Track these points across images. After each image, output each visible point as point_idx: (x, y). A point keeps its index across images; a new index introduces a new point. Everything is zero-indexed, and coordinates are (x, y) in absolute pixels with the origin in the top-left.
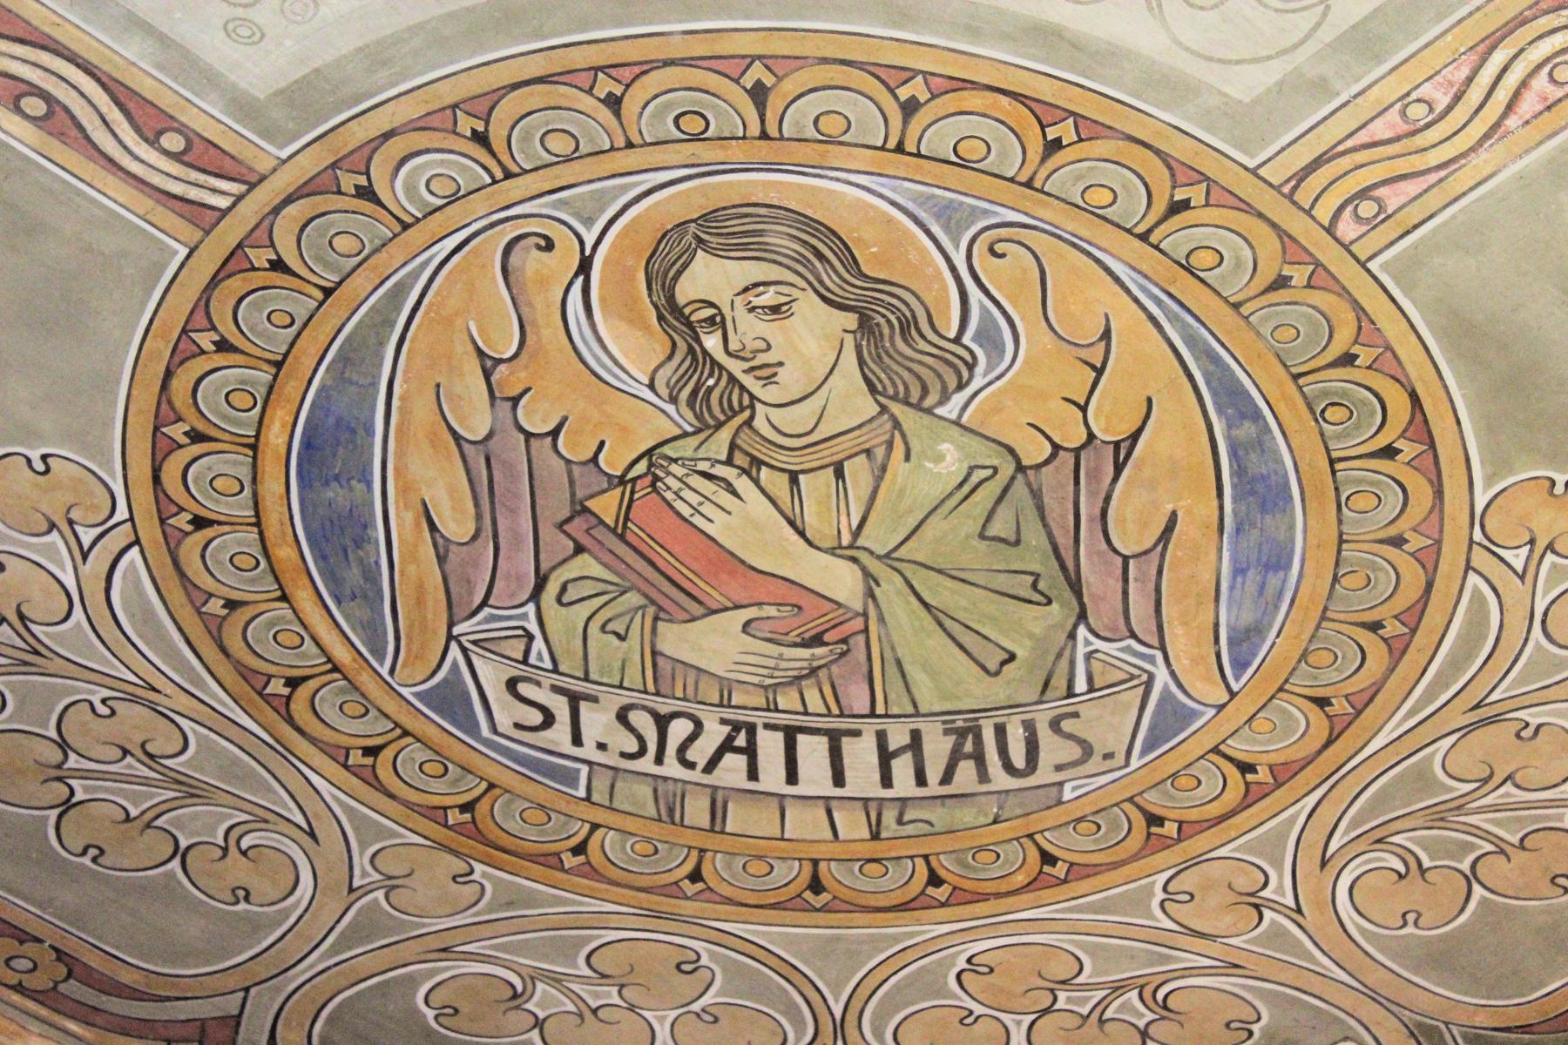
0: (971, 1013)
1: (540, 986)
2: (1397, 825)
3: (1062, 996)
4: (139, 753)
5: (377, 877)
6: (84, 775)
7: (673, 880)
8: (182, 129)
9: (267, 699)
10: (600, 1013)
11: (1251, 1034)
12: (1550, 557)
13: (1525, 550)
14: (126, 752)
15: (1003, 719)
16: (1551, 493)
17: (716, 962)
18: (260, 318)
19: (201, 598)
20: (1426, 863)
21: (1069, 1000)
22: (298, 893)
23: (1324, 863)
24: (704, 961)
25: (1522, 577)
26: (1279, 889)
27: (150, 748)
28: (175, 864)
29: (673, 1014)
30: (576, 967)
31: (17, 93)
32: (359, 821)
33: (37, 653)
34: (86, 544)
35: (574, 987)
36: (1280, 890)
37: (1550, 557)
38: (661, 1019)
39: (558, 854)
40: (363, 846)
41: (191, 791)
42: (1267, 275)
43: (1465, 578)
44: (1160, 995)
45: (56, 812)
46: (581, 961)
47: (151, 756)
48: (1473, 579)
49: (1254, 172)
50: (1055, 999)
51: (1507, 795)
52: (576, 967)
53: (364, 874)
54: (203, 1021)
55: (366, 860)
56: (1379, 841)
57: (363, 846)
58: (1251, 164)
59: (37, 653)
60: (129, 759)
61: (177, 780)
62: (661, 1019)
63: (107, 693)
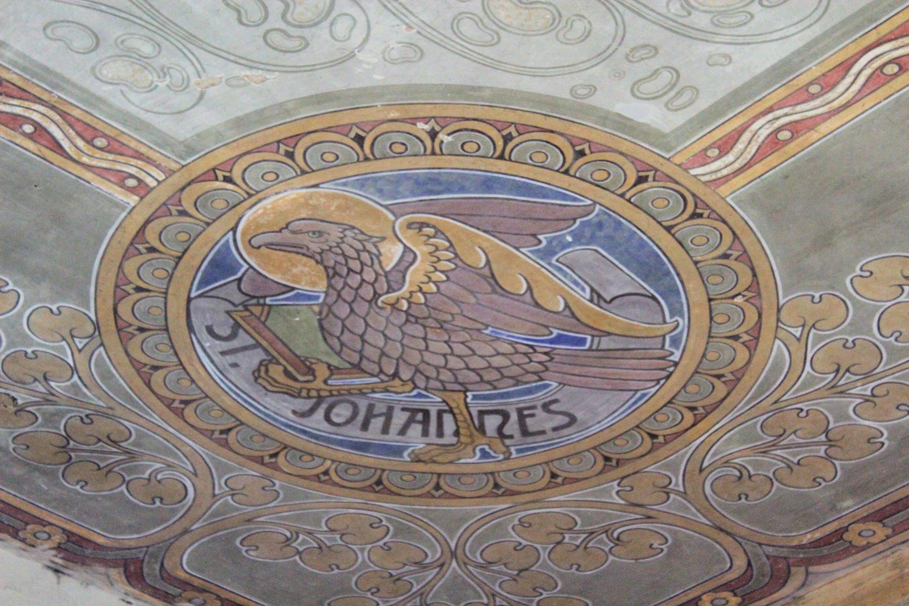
0: (520, 544)
1: (301, 537)
2: (736, 455)
3: (567, 536)
4: (105, 440)
5: (227, 489)
6: (73, 450)
7: (521, 137)
8: (105, 136)
12: (813, 331)
13: (800, 329)
15: (399, 438)
16: (813, 302)
17: (390, 522)
19: (209, 434)
20: (752, 472)
21: (571, 538)
22: (188, 497)
24: (384, 523)
25: (799, 340)
26: (678, 483)
28: (124, 488)
29: (369, 546)
30: (546, 238)
31: (14, 121)
32: (218, 464)
35: (319, 536)
36: (677, 485)
37: (813, 331)
38: (362, 550)
39: (262, 457)
40: (220, 477)
43: (774, 342)
44: (615, 535)
45: (63, 467)
46: (323, 524)
47: (114, 442)
48: (777, 342)
49: (669, 159)
50: (564, 538)
51: (792, 440)
52: (546, 238)
54: (126, 560)
55: (223, 481)
56: (726, 462)
57: (220, 477)
58: (667, 156)
61: (127, 452)
62: (362, 550)
63: (88, 412)
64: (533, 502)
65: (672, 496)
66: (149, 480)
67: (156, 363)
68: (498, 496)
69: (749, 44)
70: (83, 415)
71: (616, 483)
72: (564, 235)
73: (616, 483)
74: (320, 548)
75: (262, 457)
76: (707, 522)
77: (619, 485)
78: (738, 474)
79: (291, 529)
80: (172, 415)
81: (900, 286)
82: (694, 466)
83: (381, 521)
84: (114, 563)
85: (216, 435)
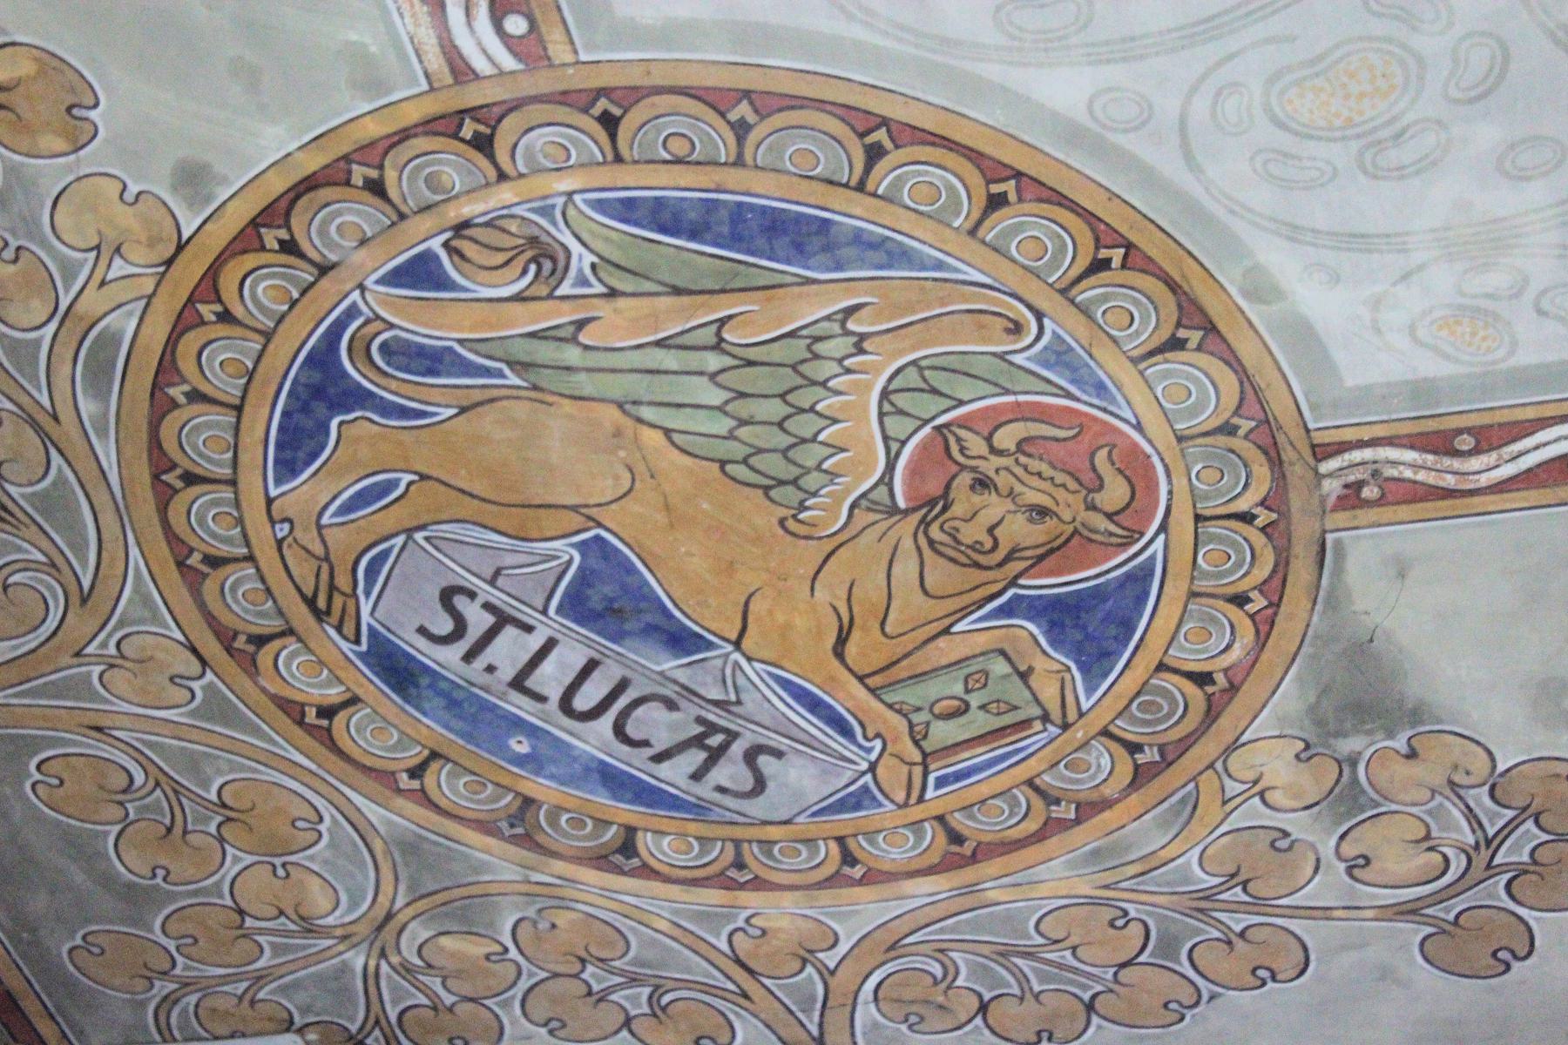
24: (323, 828)
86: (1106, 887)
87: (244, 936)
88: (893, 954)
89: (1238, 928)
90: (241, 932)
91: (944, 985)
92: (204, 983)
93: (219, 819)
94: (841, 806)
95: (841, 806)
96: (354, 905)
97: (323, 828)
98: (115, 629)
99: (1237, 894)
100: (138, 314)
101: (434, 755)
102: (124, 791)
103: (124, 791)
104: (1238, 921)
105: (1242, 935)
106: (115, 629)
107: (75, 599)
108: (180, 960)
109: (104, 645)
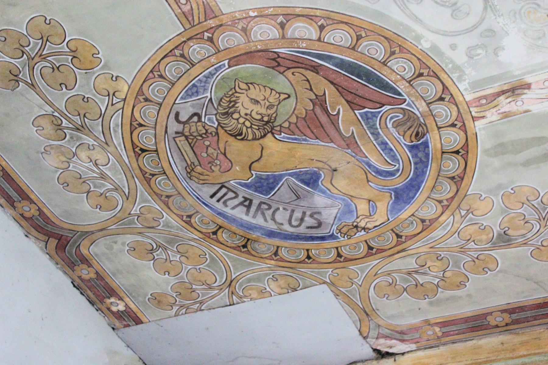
0: (266, 289)
4: (94, 162)
9: (134, 152)
10: (172, 262)
11: (273, 276)
14: (91, 161)
18: (196, 50)
19: (144, 173)
23: (375, 275)
24: (207, 256)
25: (462, 217)
27: (97, 162)
29: (190, 267)
33: (83, 127)
34: (114, 102)
39: (183, 216)
41: (103, 176)
42: (171, 199)
47: (96, 164)
53: (136, 211)
56: (389, 274)
59: (83, 127)
60: (91, 163)
64: (291, 268)
65: (354, 286)
66: (102, 194)
67: (143, 123)
68: (373, 255)
69: (326, 188)
70: (91, 144)
71: (331, 270)
72: (449, 69)
73: (331, 270)
74: (166, 260)
75: (183, 216)
76: (361, 306)
77: (332, 271)
78: (391, 282)
79: (158, 244)
80: (133, 154)
81: (523, 203)
82: (373, 272)
83: (206, 255)
84: (49, 235)
85: (185, 218)
86: (431, 248)
87: (60, 129)
88: (376, 277)
89: (476, 256)
90: (16, 78)
91: (394, 285)
92: (187, 306)
93: (179, 256)
94: (80, 130)
95: (80, 130)
96: (221, 278)
97: (207, 256)
98: (138, 206)
99: (65, 123)
100: (470, 190)
101: (220, 227)
102: (152, 250)
103: (152, 250)
104: (475, 254)
105: (477, 258)
106: (138, 206)
107: (125, 198)
108: (177, 299)
109: (136, 211)
